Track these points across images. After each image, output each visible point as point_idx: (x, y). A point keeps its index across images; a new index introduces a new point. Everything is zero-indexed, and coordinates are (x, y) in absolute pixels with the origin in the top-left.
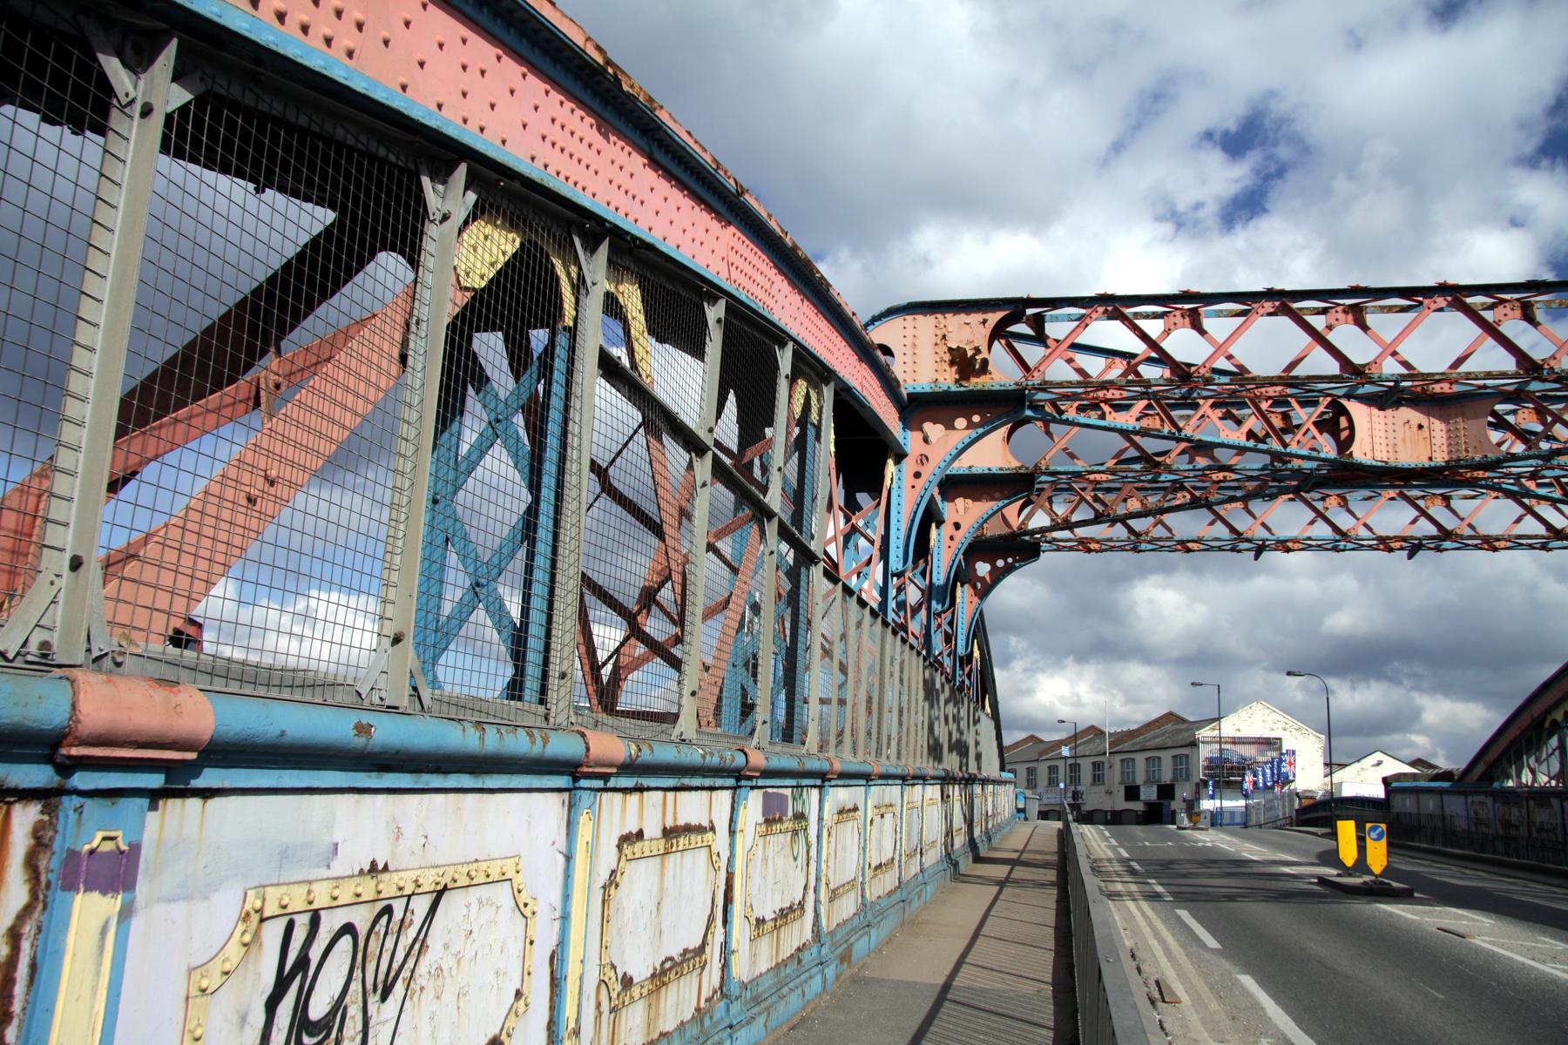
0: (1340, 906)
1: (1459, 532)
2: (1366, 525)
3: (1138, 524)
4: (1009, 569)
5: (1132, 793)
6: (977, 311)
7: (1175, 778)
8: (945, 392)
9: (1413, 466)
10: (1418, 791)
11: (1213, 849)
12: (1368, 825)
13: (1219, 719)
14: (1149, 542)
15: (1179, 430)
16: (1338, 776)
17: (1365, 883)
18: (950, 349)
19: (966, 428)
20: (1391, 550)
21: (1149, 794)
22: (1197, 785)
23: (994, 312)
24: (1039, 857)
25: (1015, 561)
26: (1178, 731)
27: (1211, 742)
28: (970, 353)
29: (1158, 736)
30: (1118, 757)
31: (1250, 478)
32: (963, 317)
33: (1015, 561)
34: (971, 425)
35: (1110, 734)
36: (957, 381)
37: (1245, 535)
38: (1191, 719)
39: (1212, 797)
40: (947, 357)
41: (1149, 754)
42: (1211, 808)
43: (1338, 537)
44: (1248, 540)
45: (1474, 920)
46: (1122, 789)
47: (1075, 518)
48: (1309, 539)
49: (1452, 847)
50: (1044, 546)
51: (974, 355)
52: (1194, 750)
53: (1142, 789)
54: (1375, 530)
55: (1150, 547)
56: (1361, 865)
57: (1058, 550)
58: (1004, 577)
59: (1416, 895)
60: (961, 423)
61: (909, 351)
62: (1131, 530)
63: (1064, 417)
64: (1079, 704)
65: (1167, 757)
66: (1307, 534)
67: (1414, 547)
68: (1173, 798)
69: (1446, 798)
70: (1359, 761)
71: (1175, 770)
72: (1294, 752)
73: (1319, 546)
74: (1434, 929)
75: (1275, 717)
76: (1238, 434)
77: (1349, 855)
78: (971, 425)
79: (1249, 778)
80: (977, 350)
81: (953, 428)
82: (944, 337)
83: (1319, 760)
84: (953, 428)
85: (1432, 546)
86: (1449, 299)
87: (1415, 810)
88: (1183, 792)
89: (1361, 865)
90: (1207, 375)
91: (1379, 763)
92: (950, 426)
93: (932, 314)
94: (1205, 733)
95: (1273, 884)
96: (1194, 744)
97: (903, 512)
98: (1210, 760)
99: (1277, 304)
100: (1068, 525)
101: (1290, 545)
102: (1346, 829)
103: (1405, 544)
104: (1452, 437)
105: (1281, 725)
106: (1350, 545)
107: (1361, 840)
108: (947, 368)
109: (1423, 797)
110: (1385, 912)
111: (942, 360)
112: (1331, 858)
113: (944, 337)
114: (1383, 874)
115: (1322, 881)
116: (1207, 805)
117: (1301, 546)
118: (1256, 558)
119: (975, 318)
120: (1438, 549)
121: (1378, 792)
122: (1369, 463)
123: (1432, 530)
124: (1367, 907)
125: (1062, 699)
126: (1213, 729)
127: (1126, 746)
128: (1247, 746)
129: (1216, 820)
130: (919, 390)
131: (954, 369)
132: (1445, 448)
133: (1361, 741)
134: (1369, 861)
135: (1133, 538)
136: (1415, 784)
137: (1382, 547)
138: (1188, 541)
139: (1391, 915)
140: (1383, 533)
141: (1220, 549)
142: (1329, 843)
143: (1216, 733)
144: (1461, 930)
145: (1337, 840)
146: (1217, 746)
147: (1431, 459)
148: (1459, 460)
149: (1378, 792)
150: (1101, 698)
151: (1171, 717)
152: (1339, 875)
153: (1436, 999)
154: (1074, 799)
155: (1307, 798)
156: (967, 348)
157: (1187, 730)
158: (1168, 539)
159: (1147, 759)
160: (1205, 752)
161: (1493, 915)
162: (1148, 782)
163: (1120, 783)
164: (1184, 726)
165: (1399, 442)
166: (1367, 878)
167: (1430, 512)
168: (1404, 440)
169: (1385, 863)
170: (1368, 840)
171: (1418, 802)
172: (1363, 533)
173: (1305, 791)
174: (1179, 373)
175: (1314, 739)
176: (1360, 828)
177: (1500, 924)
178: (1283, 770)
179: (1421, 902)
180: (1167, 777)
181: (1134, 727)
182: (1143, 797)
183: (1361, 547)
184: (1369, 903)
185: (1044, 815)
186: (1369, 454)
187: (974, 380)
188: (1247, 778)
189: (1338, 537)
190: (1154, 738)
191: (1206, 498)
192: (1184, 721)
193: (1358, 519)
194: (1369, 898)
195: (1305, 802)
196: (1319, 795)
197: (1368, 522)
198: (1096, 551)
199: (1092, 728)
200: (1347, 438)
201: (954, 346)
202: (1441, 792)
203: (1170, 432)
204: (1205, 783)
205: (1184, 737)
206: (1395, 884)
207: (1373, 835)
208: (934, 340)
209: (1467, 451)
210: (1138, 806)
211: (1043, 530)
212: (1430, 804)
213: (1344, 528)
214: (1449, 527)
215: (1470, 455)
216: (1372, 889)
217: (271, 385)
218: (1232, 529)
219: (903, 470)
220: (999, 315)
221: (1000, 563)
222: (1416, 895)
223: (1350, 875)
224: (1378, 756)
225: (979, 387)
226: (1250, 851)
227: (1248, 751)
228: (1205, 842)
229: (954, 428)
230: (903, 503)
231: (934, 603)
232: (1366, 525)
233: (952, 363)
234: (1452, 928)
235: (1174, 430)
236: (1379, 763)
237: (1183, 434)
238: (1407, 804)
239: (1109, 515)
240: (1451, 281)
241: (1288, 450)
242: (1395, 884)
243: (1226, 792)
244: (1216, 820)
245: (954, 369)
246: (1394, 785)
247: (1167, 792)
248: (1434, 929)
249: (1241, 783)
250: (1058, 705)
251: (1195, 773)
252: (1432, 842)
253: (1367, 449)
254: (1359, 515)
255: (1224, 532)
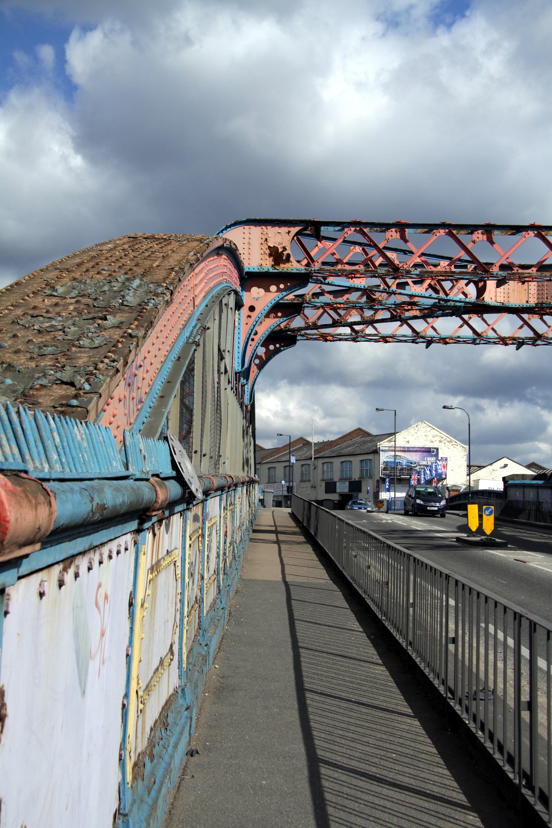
0: (467, 551)
1: (546, 335)
2: (493, 329)
3: (357, 328)
4: (277, 351)
5: (330, 487)
6: (285, 226)
7: (362, 477)
8: (266, 272)
9: (517, 306)
10: (524, 486)
11: (393, 524)
12: (484, 507)
13: (394, 434)
14: (363, 337)
15: (389, 287)
16: (474, 477)
17: (481, 540)
18: (269, 247)
19: (276, 292)
20: (506, 344)
21: (343, 488)
22: (378, 481)
23: (294, 227)
24: (288, 529)
25: (281, 346)
26: (365, 443)
27: (389, 451)
28: (280, 250)
29: (350, 446)
30: (321, 461)
31: (425, 309)
32: (277, 229)
33: (281, 346)
34: (279, 290)
35: (315, 444)
36: (273, 266)
37: (421, 334)
38: (374, 434)
39: (388, 490)
40: (268, 252)
41: (343, 459)
42: (387, 498)
43: (475, 337)
44: (423, 337)
45: (534, 556)
46: (323, 484)
47: (320, 323)
48: (459, 337)
49: (540, 521)
50: (298, 338)
51: (283, 251)
52: (376, 456)
53: (338, 484)
54: (498, 332)
55: (363, 339)
56: (480, 531)
57: (307, 339)
58: (274, 356)
59: (509, 546)
60: (273, 288)
61: (246, 247)
62: (353, 330)
63: (327, 281)
64: (287, 417)
65: (356, 461)
66: (457, 334)
67: (520, 343)
68: (360, 491)
69: (540, 491)
70: (491, 464)
71: (362, 471)
72: (446, 460)
73: (464, 341)
74: (513, 560)
75: (434, 432)
76: (421, 288)
77: (474, 525)
78: (279, 290)
79: (415, 476)
80: (285, 249)
81: (269, 291)
82: (266, 240)
83: (464, 463)
84: (269, 291)
85: (530, 343)
86: (536, 232)
87: (522, 499)
88: (368, 486)
89: (480, 531)
90: (408, 269)
91: (506, 466)
92: (267, 290)
93: (260, 226)
94: (384, 444)
95: (431, 542)
96: (376, 452)
97: (241, 338)
98: (386, 463)
99: (447, 231)
100: (315, 326)
101: (448, 340)
102: (473, 509)
103: (515, 342)
104: (540, 290)
105: (437, 439)
106: (482, 342)
107: (481, 517)
108: (268, 258)
109: (527, 490)
110: (490, 553)
111: (265, 253)
112: (465, 528)
113: (266, 240)
114: (492, 534)
115: (458, 539)
116: (384, 496)
117: (454, 341)
118: (427, 347)
119: (284, 230)
120: (534, 345)
121: (499, 486)
122: (493, 304)
123: (531, 334)
124: (481, 551)
125: (276, 414)
126: (390, 441)
127: (327, 453)
128: (413, 454)
129: (390, 507)
130: (252, 270)
131: (271, 258)
132: (535, 296)
133: (493, 448)
134: (484, 528)
135: (353, 334)
136: (522, 482)
137: (501, 342)
138: (387, 337)
139: (493, 555)
140: (503, 335)
141: (405, 341)
142: (462, 521)
143: (393, 444)
144: (525, 560)
145: (467, 518)
146: (393, 453)
147: (527, 302)
148: (542, 303)
149: (499, 486)
150: (306, 414)
151: (359, 432)
152: (468, 536)
153: (502, 583)
154: (288, 492)
155: (454, 491)
156: (279, 247)
157: (371, 441)
158: (375, 335)
159: (361, 461)
160: (384, 457)
161: (545, 554)
162: (342, 479)
163: (322, 480)
164: (369, 438)
165: (510, 291)
166: (483, 537)
167: (530, 322)
168: (514, 291)
169: (493, 528)
170: (484, 515)
171: (524, 494)
172: (491, 334)
173: (454, 486)
174: (393, 267)
175: (461, 448)
176: (480, 510)
177: (546, 557)
178: (440, 471)
179: (511, 549)
180: (356, 476)
181: (333, 438)
182: (338, 490)
183: (489, 343)
184: (482, 550)
185: (278, 504)
186: (494, 299)
187: (282, 266)
188: (413, 477)
189: (475, 337)
190: (347, 447)
191: (400, 316)
192: (369, 435)
193: (489, 325)
194: (483, 548)
195: (453, 494)
196: (463, 489)
197: (494, 327)
198: (331, 341)
199: (301, 440)
200: (482, 286)
201: (272, 246)
202: (537, 487)
203: (384, 289)
204: (384, 480)
205: (369, 447)
206: (498, 540)
207: (487, 513)
208: (261, 241)
209: (547, 298)
210: (335, 497)
211: (300, 329)
212: (531, 495)
213: (479, 331)
214: (540, 332)
215: (549, 301)
216: (485, 543)
217: (138, 364)
218: (414, 330)
219: (242, 314)
220: (297, 229)
221: (272, 347)
222: (509, 546)
223: (474, 536)
224: (505, 461)
225: (285, 270)
226: (417, 525)
227: (414, 457)
228: (387, 520)
229: (270, 291)
230: (241, 333)
231: (242, 378)
232: (493, 329)
233: (270, 255)
234: (522, 559)
235: (386, 288)
236: (506, 466)
237: (391, 289)
238: (516, 495)
239: (341, 322)
240: (538, 223)
241: (448, 298)
242: (498, 540)
243: (398, 486)
244: (390, 507)
245: (271, 258)
246: (510, 482)
247: (356, 486)
248: (513, 560)
249: (409, 480)
250: (272, 418)
251: (376, 473)
252: (529, 519)
253: (493, 296)
254: (489, 323)
255: (408, 332)
